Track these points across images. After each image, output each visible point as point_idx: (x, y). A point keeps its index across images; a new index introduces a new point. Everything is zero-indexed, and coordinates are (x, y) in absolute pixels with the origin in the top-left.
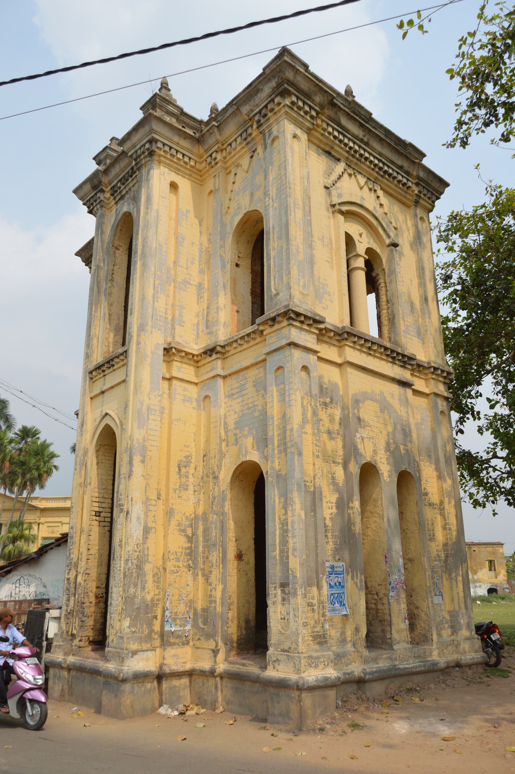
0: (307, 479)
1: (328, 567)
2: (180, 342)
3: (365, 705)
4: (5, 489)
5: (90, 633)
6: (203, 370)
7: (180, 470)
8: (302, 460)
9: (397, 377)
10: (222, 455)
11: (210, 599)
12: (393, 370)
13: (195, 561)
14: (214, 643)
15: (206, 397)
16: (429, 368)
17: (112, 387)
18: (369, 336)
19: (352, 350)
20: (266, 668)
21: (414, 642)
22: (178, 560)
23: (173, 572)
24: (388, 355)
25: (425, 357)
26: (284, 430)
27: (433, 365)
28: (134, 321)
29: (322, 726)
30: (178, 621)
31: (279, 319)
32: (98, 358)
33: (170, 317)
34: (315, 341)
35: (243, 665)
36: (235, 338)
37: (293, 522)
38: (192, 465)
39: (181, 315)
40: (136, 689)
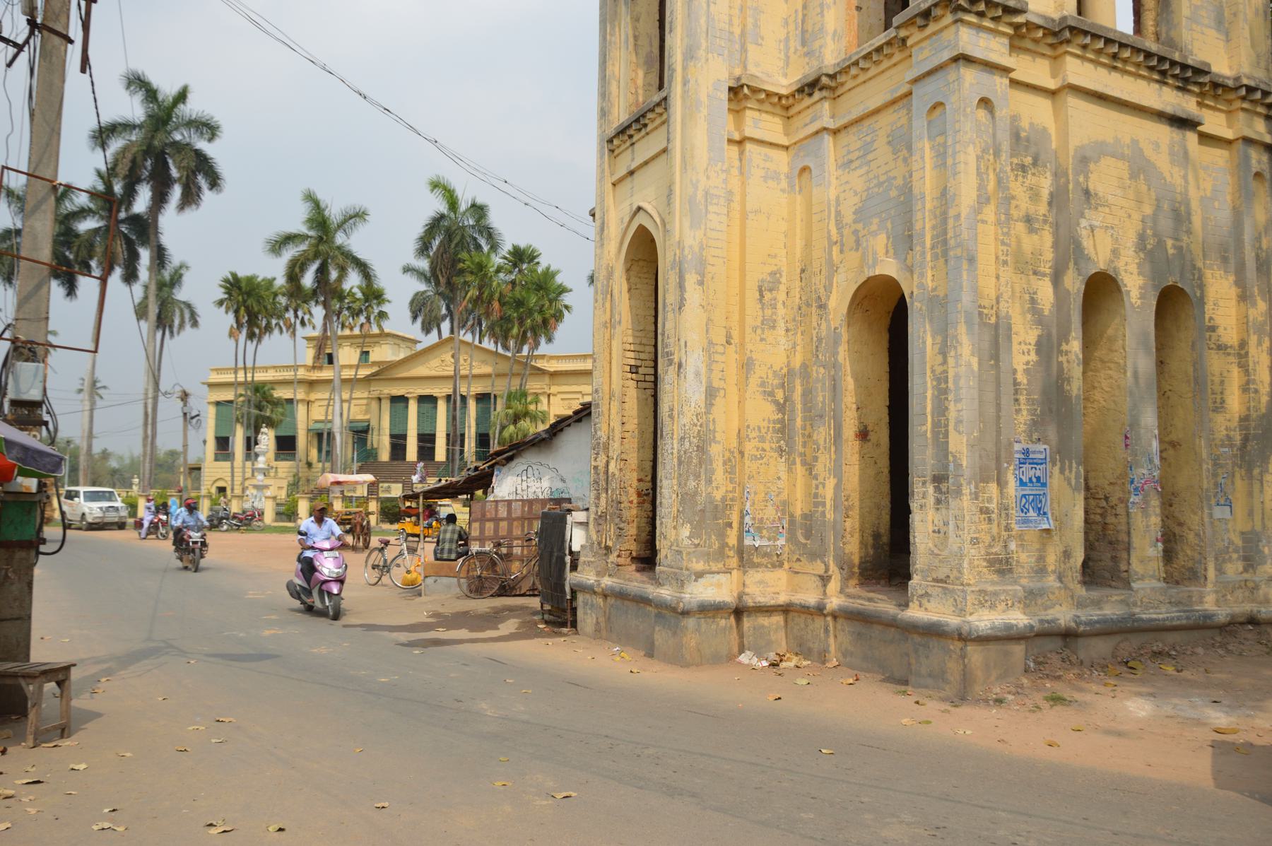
0: (986, 303)
1: (1017, 452)
2: (758, 74)
3: (1076, 671)
4: (496, 343)
5: (633, 547)
6: (797, 122)
7: (762, 296)
8: (976, 269)
9: (1169, 110)
10: (833, 269)
11: (815, 499)
12: (1160, 96)
13: (790, 441)
14: (823, 566)
15: (804, 169)
16: (1237, 88)
17: (646, 163)
18: (1116, 31)
19: (1078, 61)
20: (907, 605)
21: (1171, 579)
22: (762, 439)
23: (755, 458)
24: (1151, 69)
25: (1230, 68)
26: (942, 219)
27: (1245, 81)
28: (676, 42)
29: (1000, 696)
30: (765, 532)
31: (937, 12)
32: (621, 115)
33: (737, 31)
34: (1006, 50)
35: (870, 600)
36: (854, 59)
37: (957, 377)
38: (783, 288)
39: (756, 26)
40: (704, 626)
